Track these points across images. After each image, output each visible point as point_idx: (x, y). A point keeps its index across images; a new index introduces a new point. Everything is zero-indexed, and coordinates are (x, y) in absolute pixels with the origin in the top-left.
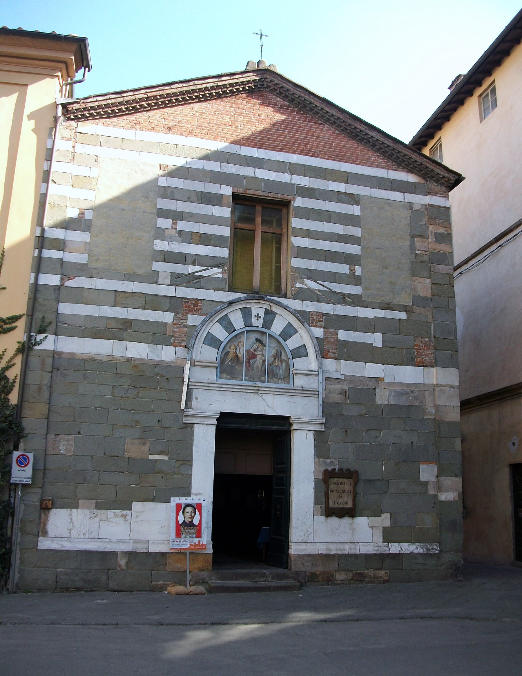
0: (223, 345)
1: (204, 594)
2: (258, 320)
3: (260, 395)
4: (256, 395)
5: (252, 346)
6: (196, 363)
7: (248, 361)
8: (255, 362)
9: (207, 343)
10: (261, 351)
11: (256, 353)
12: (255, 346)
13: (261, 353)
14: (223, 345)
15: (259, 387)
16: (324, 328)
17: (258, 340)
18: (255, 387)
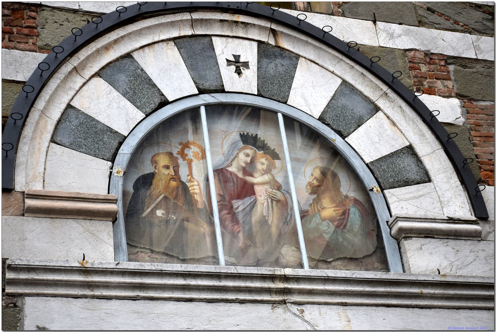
0: (127, 149)
1: (391, 216)
2: (239, 72)
3: (294, 308)
4: (280, 310)
5: (231, 158)
6: (30, 202)
7: (226, 205)
8: (253, 205)
9: (66, 141)
10: (268, 171)
11: (249, 179)
12: (243, 158)
13: (266, 178)
14: (127, 149)
15: (286, 278)
16: (459, 96)
17: (248, 140)
18: (272, 278)
